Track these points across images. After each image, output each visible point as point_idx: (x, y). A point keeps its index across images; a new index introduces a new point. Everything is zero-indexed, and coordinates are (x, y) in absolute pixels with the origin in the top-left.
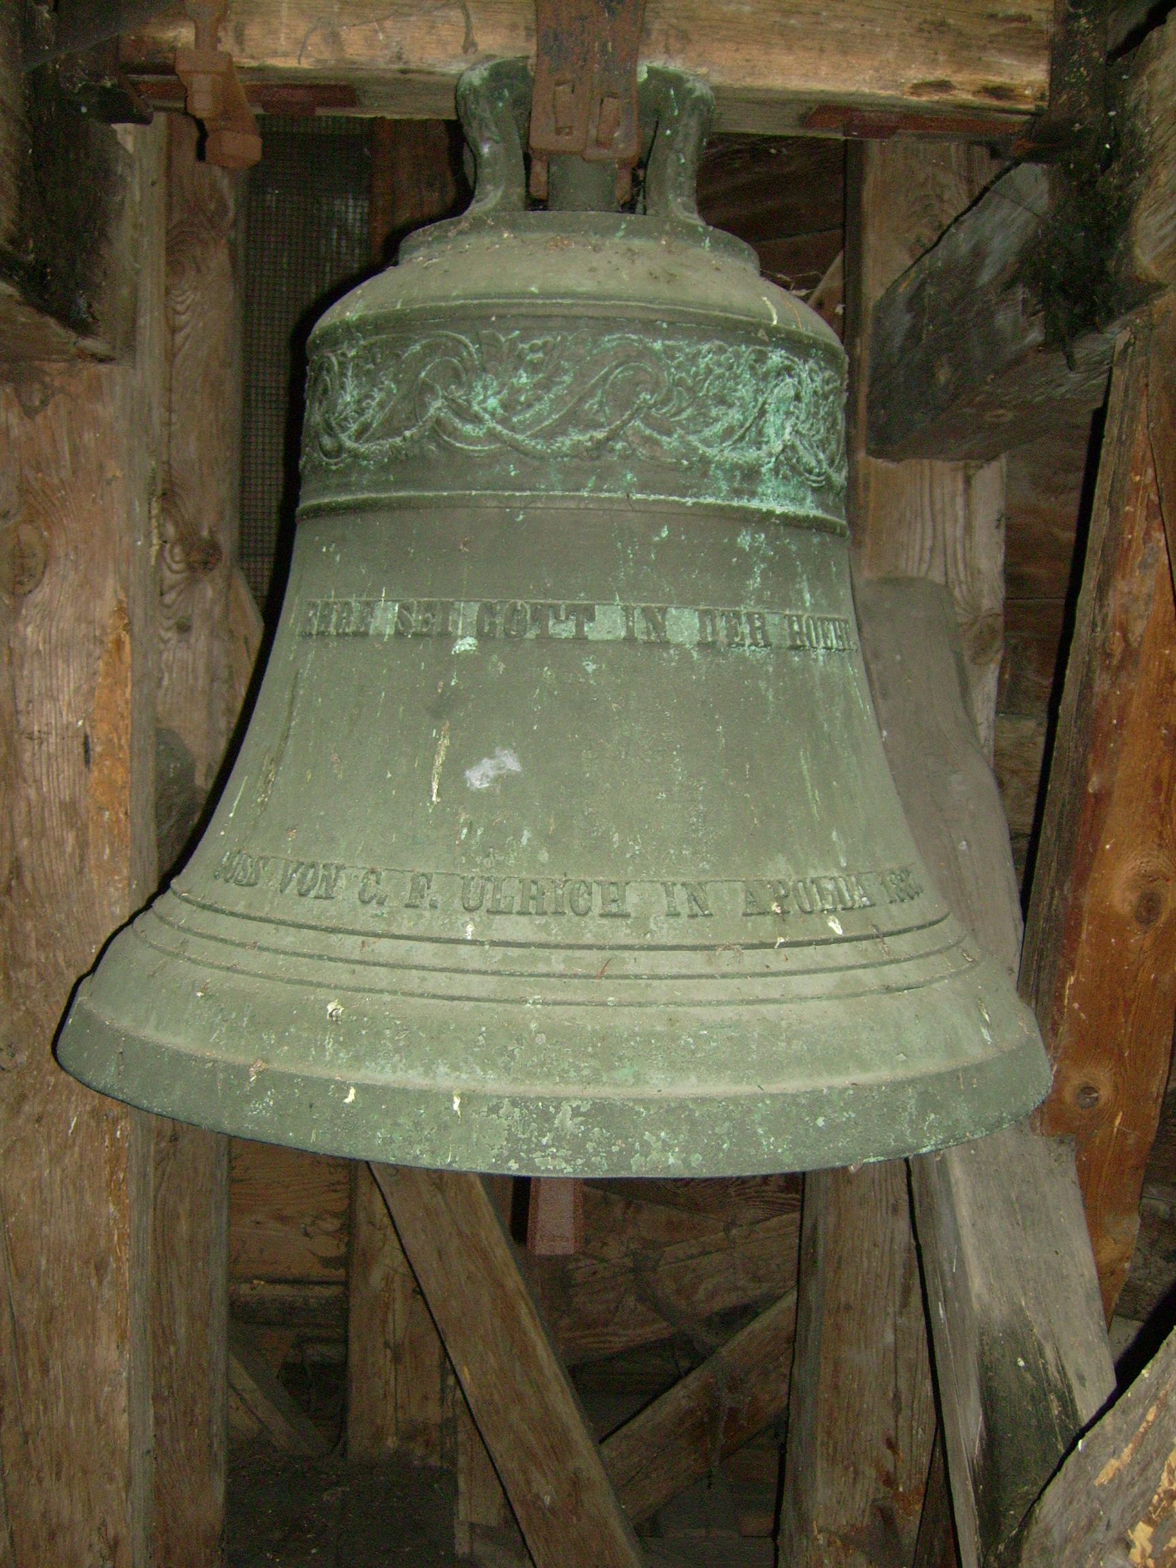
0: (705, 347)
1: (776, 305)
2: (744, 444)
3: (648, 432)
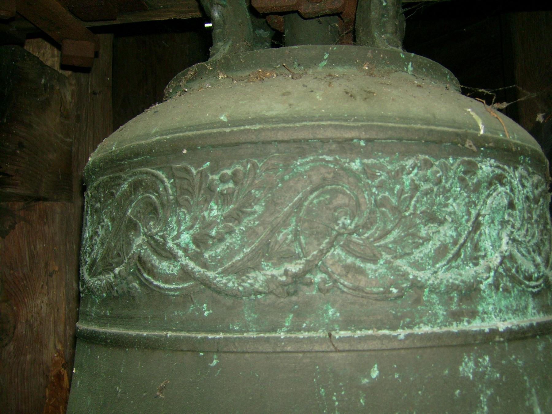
0: (409, 163)
1: (481, 118)
2: (459, 261)
3: (350, 260)
